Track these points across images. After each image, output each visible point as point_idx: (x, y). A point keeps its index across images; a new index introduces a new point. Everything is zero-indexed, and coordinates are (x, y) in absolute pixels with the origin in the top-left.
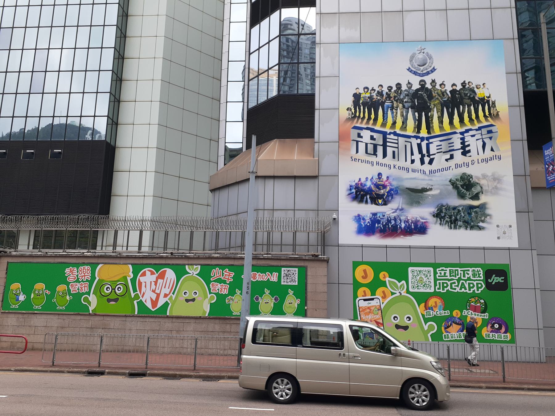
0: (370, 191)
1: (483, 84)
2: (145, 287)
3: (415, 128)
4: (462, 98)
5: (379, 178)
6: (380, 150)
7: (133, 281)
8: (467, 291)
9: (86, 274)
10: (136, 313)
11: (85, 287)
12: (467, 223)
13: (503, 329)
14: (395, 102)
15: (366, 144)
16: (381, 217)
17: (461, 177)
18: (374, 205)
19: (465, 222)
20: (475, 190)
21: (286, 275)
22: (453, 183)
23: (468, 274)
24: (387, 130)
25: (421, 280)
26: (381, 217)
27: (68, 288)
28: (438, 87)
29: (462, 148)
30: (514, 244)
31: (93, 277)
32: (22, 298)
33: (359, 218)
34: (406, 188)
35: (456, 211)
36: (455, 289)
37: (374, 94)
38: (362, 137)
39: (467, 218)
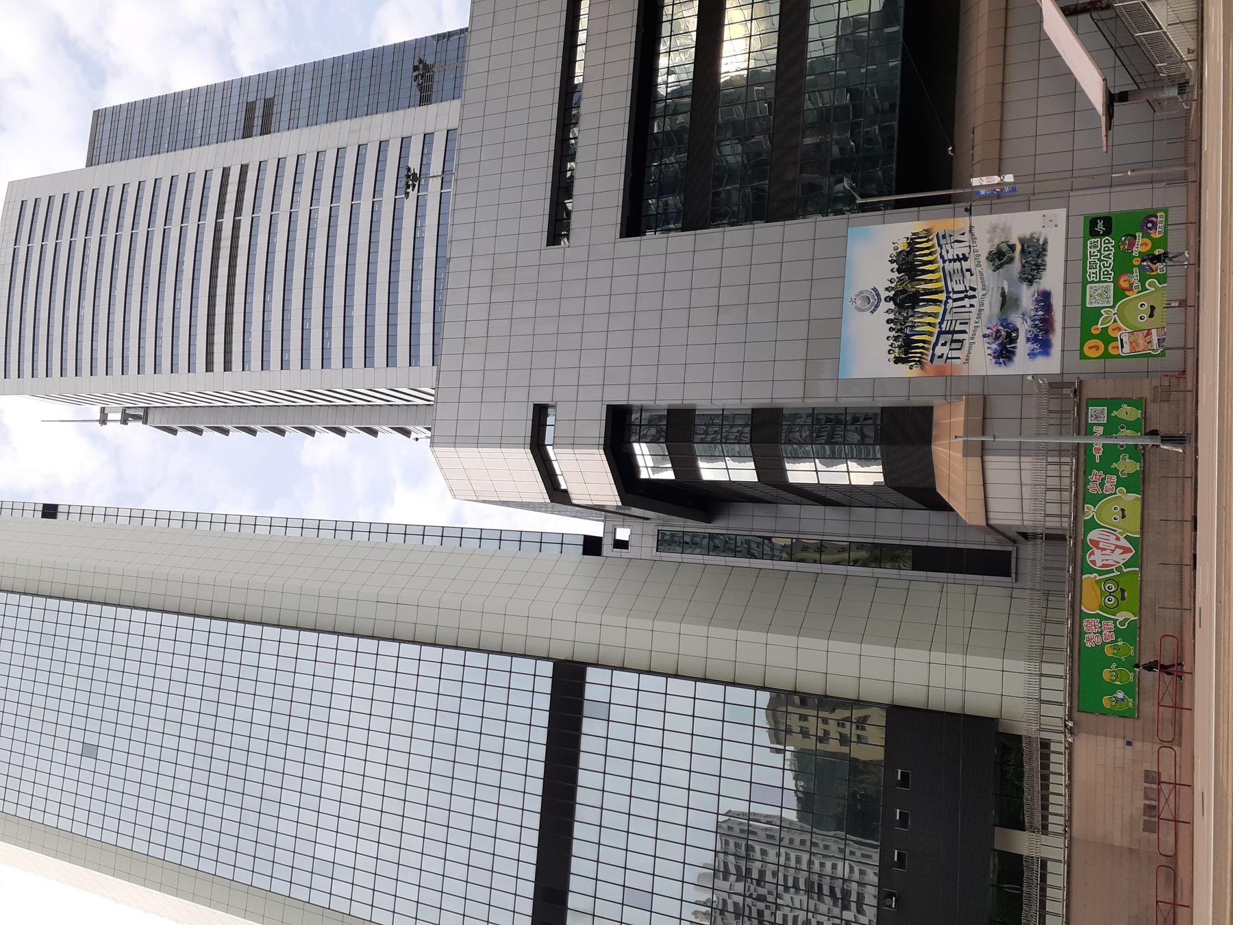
0: (1003, 346)
1: (894, 244)
2: (1107, 560)
3: (936, 305)
4: (907, 263)
5: (989, 336)
6: (956, 336)
7: (1100, 573)
8: (1112, 252)
9: (1093, 624)
10: (1138, 569)
11: (1107, 625)
12: (1039, 254)
13: (1154, 219)
14: (907, 324)
15: (950, 349)
16: (1031, 333)
17: (991, 261)
18: (1018, 341)
19: (1038, 256)
20: (1005, 248)
21: (1096, 418)
22: (997, 268)
23: (1094, 252)
24: (936, 331)
25: (1100, 295)
26: (1031, 333)
27: (1108, 643)
28: (893, 285)
29: (960, 261)
30: (1061, 213)
31: (1097, 616)
32: (1120, 695)
33: (1032, 355)
34: (1001, 310)
35: (1026, 265)
36: (1110, 264)
37: (897, 344)
38: (943, 354)
39: (1034, 255)
